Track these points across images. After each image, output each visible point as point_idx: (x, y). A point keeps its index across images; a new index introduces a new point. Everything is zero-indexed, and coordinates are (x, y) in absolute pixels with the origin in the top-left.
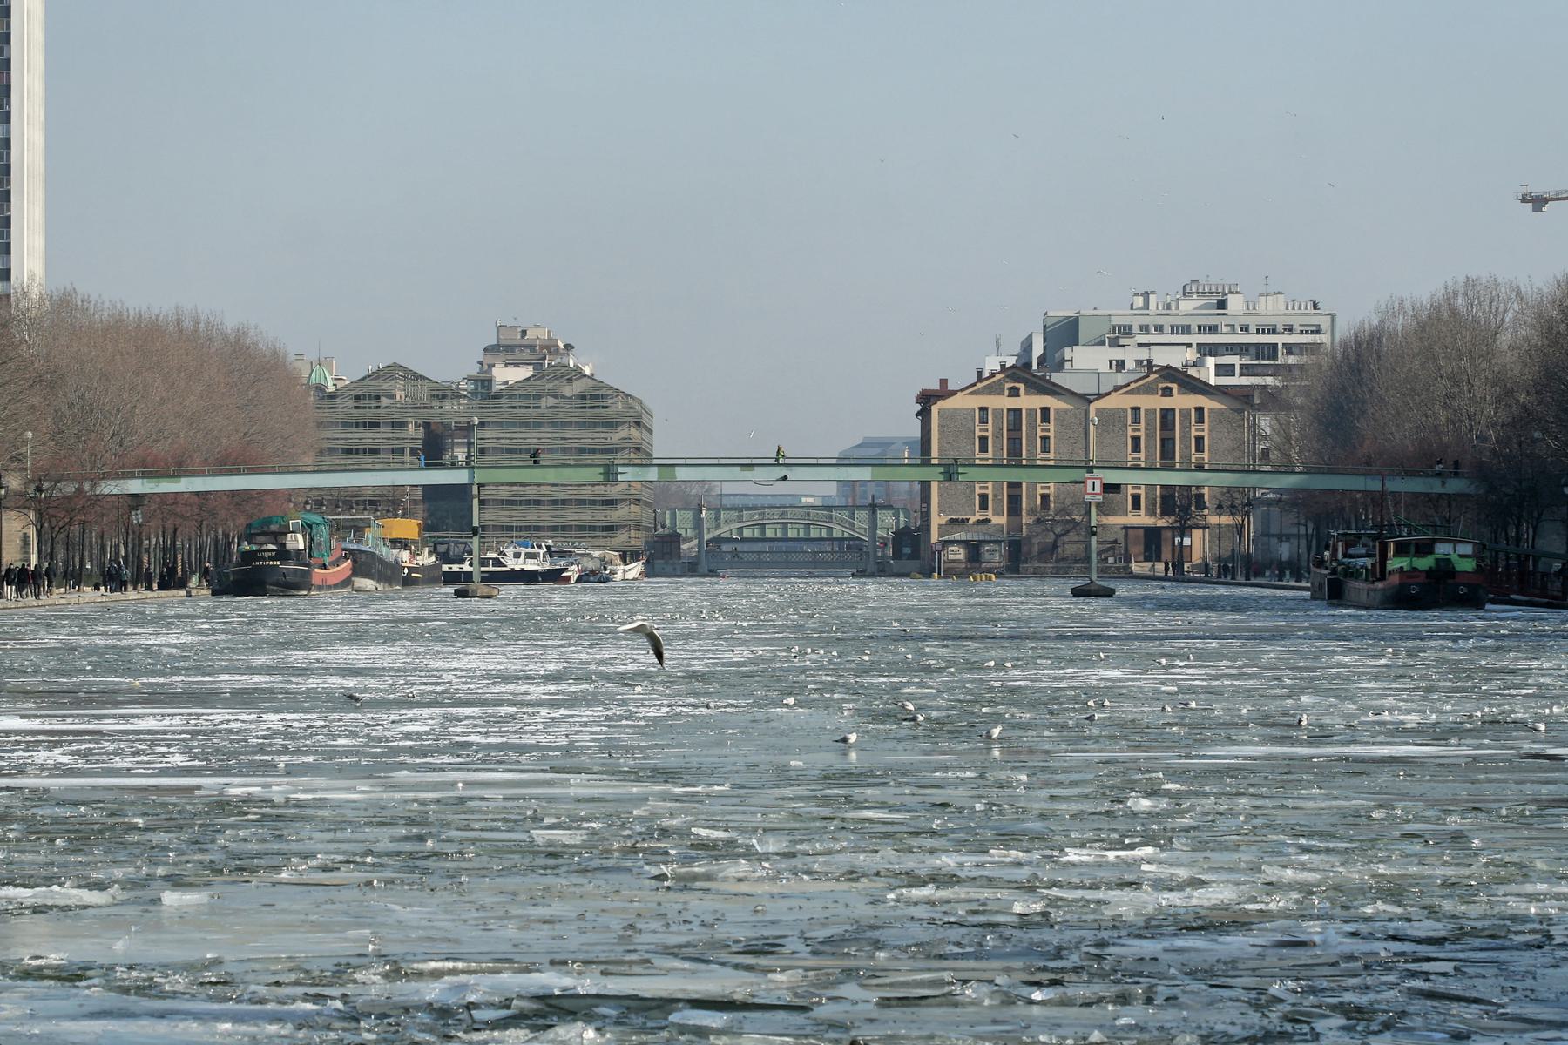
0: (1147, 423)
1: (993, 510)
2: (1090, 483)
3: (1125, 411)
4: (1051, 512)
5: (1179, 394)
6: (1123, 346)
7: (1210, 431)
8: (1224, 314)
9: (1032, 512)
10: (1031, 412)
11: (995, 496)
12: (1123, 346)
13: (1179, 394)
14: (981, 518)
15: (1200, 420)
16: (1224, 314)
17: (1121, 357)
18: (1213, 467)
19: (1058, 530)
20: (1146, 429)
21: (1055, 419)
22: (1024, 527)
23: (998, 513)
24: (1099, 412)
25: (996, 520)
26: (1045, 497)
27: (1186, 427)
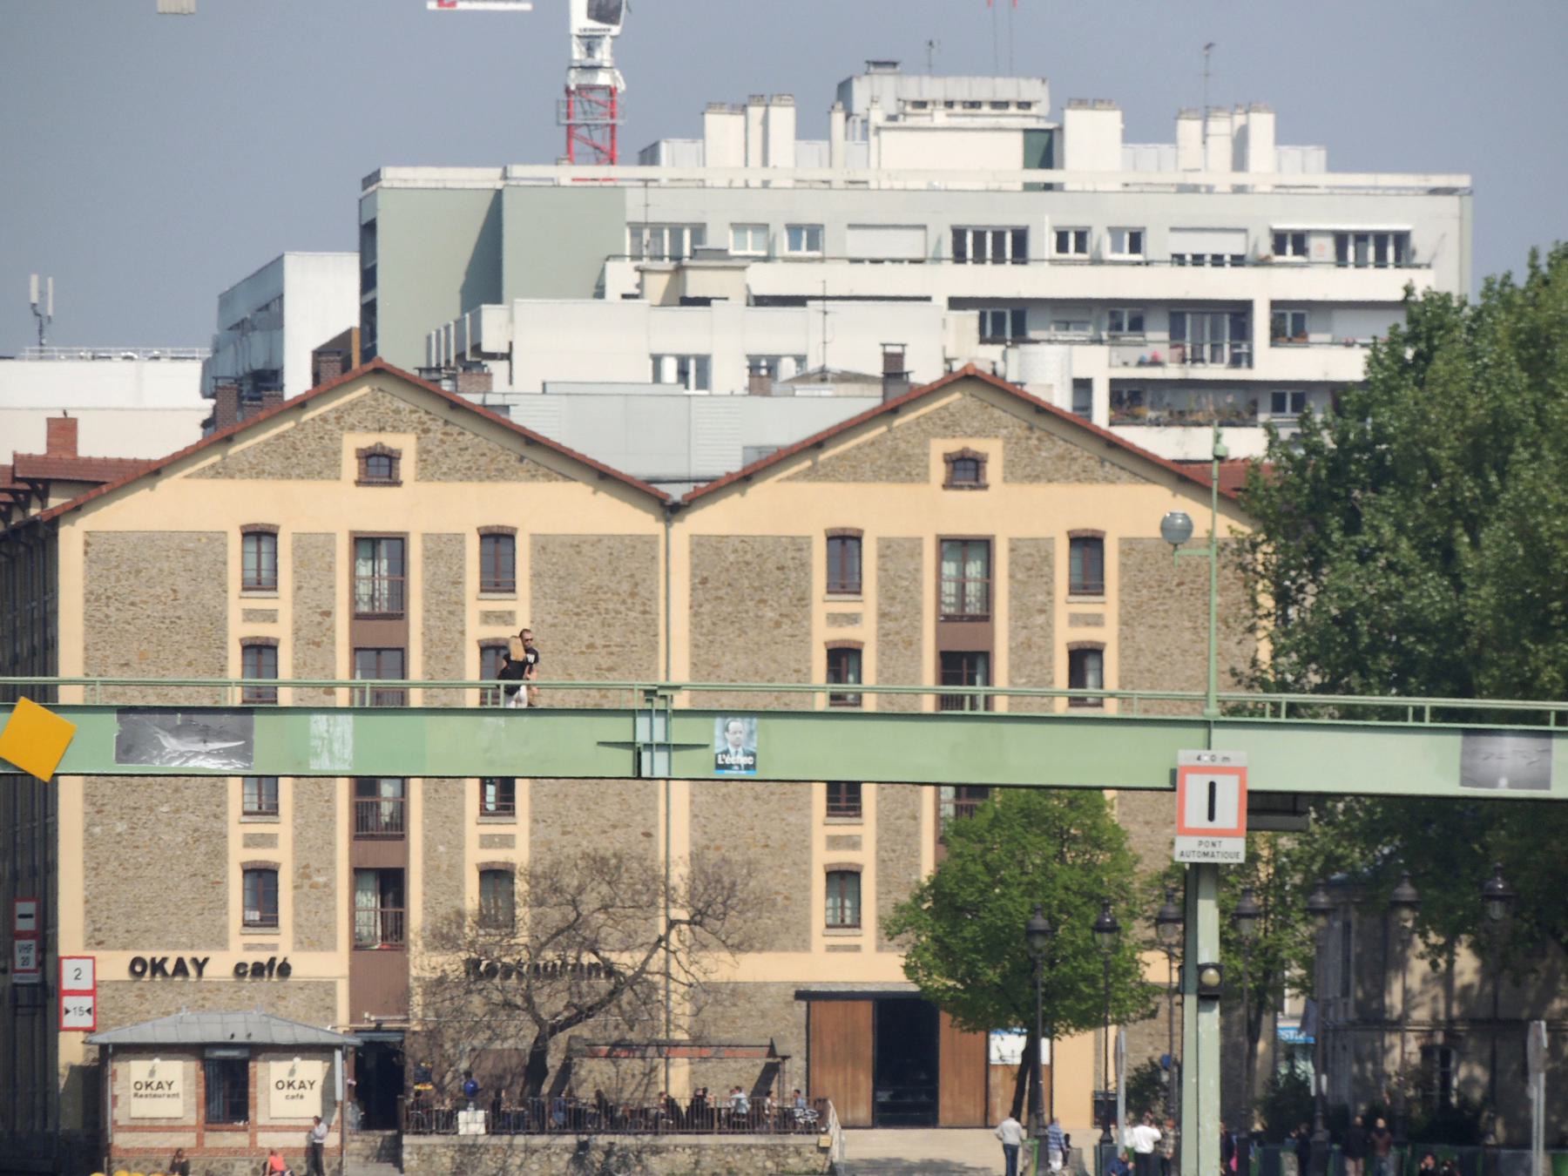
0: (887, 593)
1: (297, 926)
2: (1195, 790)
3: (800, 545)
4: (523, 938)
5: (1051, 540)
6: (704, 302)
7: (1125, 622)
8: (1048, 187)
9: (442, 939)
10: (443, 547)
11: (303, 873)
12: (704, 302)
13: (1051, 540)
14: (250, 958)
15: (1088, 581)
16: (1048, 187)
17: (692, 345)
18: (704, 703)
19: (553, 1002)
20: (883, 616)
21: (536, 576)
22: (417, 999)
23: (312, 940)
24: (699, 543)
25: (306, 966)
26: (495, 877)
27: (1033, 612)
